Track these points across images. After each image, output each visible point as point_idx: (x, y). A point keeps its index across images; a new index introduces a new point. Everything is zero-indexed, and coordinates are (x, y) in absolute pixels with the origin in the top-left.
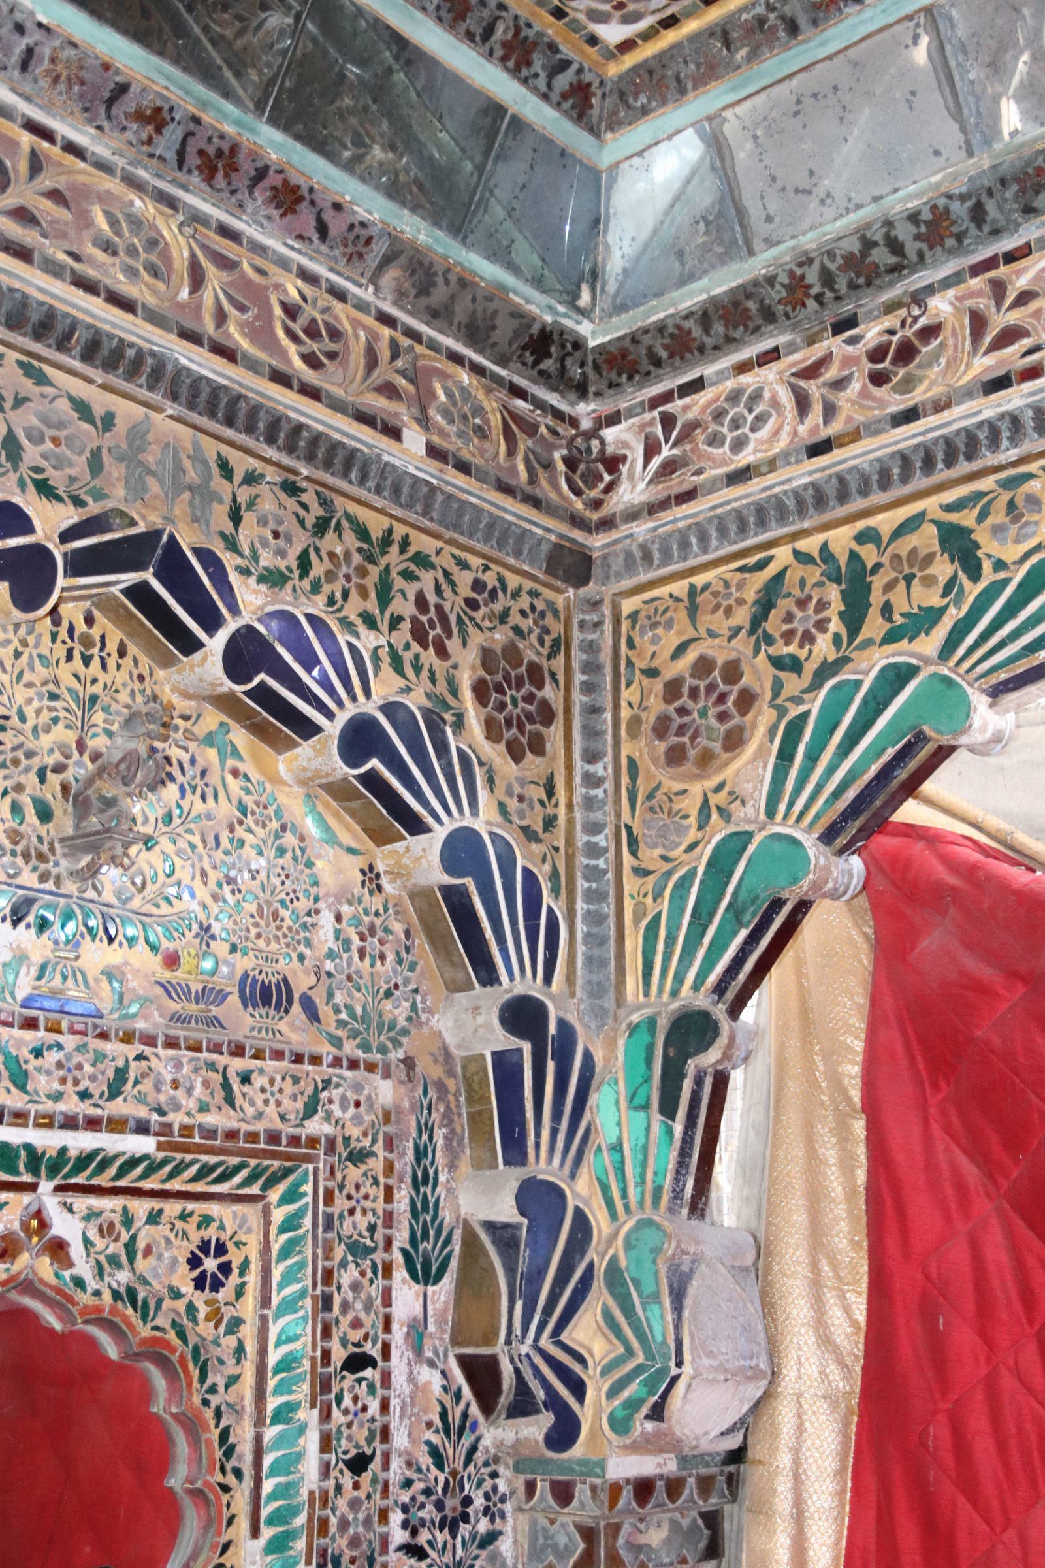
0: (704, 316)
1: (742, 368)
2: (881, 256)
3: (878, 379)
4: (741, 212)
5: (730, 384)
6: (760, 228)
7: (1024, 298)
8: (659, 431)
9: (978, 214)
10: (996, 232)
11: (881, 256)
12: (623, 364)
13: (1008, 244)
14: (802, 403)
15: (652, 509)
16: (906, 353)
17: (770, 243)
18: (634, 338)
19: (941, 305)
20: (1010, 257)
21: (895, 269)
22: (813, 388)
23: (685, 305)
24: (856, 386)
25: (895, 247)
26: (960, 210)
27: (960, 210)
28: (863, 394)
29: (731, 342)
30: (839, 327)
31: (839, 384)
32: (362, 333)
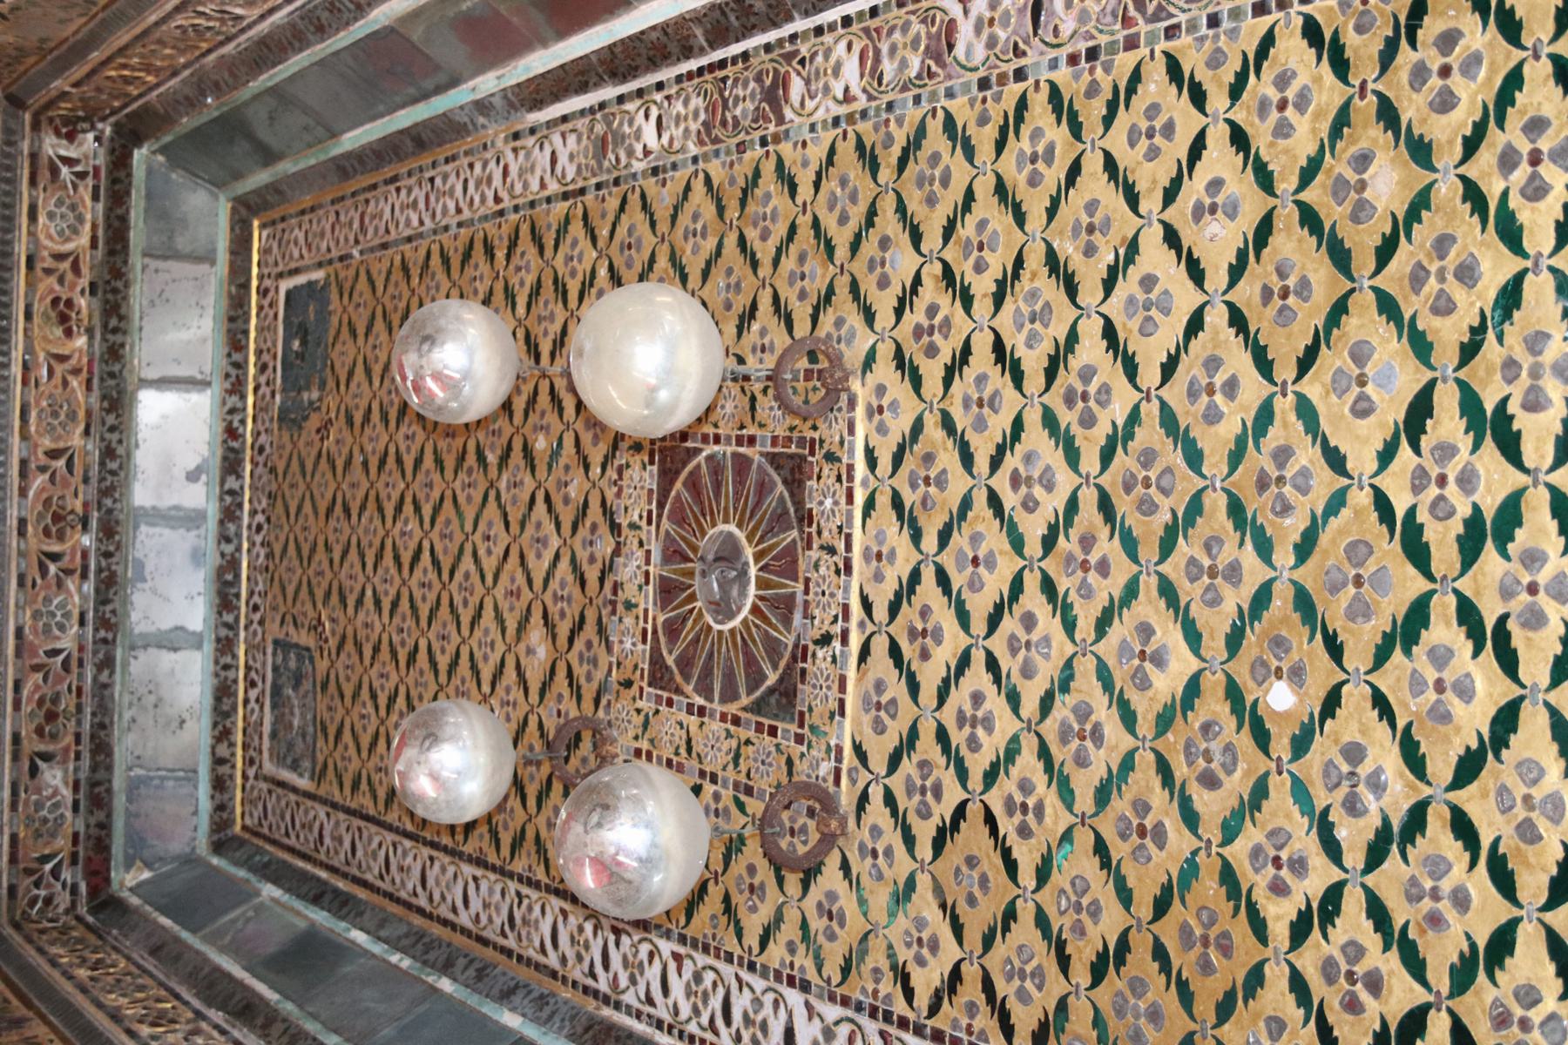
0: (124, 219)
1: (94, 227)
2: (113, 322)
3: (56, 301)
4: (165, 258)
5: (89, 217)
6: (154, 264)
7: (65, 383)
8: (79, 169)
9: (112, 375)
10: (102, 380)
11: (113, 322)
12: (120, 161)
13: (96, 381)
14: (59, 257)
15: (34, 156)
16: (63, 319)
17: (144, 268)
18: (129, 175)
19: (81, 342)
20: (89, 382)
21: (105, 326)
22: (66, 265)
23: (133, 214)
24: (57, 287)
25: (115, 331)
26: (116, 368)
27: (116, 368)
28: (52, 290)
29: (108, 226)
30: (93, 285)
31: (61, 281)
32: (150, 79)
